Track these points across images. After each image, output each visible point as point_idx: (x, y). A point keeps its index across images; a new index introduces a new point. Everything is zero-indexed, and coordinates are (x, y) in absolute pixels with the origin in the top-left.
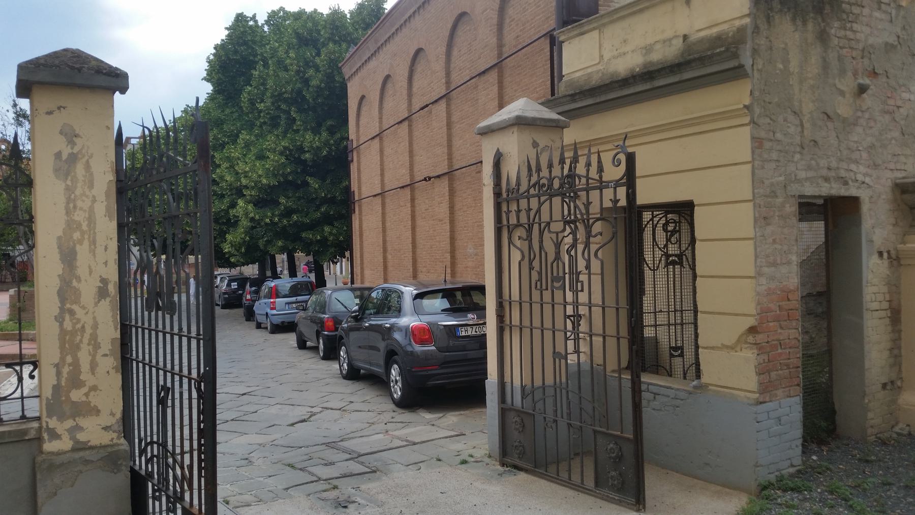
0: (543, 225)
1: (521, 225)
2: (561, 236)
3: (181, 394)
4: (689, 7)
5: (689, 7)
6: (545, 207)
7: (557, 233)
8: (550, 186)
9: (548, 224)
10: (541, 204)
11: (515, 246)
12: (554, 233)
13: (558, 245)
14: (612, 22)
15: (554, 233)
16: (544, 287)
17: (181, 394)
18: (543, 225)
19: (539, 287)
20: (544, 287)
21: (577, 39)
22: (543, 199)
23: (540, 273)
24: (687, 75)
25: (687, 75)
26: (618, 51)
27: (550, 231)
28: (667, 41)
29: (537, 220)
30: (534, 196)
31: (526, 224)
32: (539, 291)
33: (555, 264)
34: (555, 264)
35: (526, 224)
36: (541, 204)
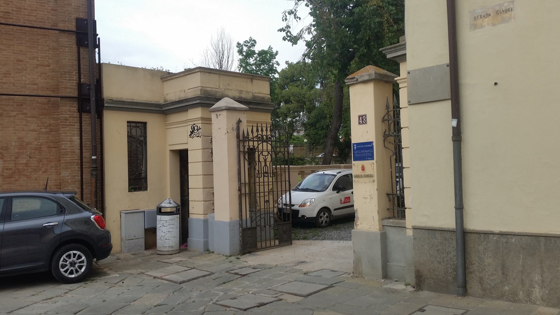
0: (260, 153)
1: (281, 152)
2: (266, 157)
3: (267, 218)
4: (252, 84)
5: (252, 84)
6: (260, 146)
7: (265, 156)
8: (263, 138)
9: (262, 152)
10: (258, 145)
11: (246, 159)
12: (264, 156)
13: (265, 161)
14: (224, 75)
15: (264, 156)
16: (260, 176)
17: (267, 218)
18: (260, 153)
19: (258, 177)
20: (260, 176)
21: (208, 74)
22: (259, 142)
23: (259, 171)
24: (259, 107)
25: (259, 107)
26: (226, 87)
27: (263, 155)
28: (248, 92)
29: (257, 149)
30: (256, 141)
31: (283, 152)
32: (272, 178)
33: (265, 167)
34: (265, 167)
35: (283, 152)
36: (258, 145)
